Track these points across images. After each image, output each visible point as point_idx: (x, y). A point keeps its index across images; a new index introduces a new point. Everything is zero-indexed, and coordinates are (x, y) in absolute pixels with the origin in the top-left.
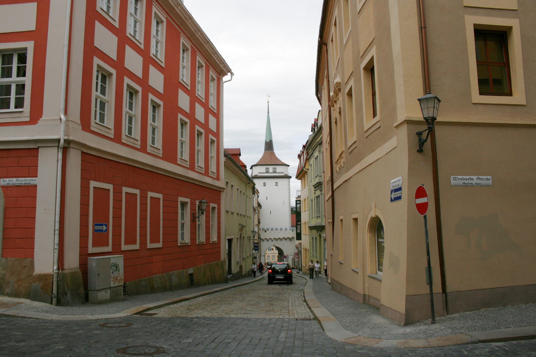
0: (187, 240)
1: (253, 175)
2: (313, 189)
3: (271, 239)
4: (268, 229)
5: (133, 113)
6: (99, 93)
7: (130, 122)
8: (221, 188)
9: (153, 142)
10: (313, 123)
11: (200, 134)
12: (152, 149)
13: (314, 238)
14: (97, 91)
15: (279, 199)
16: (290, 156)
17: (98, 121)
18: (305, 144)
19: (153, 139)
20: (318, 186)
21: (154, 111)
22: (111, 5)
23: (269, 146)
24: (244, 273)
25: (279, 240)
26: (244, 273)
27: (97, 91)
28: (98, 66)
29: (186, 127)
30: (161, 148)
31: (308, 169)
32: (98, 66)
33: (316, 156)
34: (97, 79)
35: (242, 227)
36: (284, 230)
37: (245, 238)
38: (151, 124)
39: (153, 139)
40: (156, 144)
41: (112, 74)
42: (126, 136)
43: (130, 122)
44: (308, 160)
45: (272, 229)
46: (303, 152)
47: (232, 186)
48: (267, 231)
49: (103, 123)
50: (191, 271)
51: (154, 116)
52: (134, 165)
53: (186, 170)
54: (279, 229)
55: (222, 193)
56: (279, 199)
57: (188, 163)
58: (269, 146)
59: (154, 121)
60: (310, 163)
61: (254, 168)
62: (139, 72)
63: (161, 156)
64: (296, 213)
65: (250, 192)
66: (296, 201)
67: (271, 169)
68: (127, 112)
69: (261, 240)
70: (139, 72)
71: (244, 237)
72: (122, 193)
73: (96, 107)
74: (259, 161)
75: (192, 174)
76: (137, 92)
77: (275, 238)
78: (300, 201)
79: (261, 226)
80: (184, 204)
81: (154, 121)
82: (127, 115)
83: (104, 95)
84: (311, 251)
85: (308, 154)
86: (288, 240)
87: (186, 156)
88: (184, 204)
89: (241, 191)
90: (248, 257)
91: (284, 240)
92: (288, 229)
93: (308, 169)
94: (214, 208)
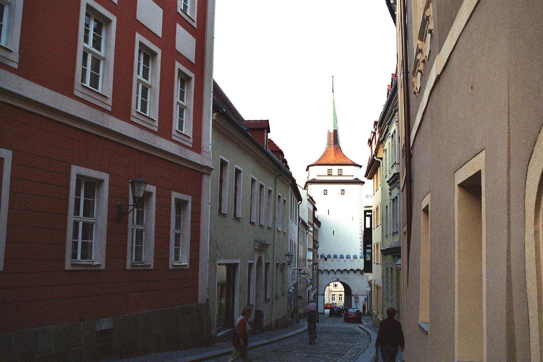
0: (148, 258)
1: (310, 179)
2: (388, 187)
3: (333, 270)
4: (329, 256)
5: (184, 104)
6: (141, 77)
7: (144, 95)
8: (203, 167)
9: (181, 127)
10: (390, 84)
11: (149, 55)
12: (177, 135)
13: (389, 269)
14: (86, 40)
15: (345, 213)
16: (358, 150)
17: (139, 110)
18: (377, 119)
19: (181, 123)
20: (393, 181)
21: (182, 86)
22: (189, 5)
23: (334, 138)
24: (265, 324)
25: (345, 274)
26: (265, 324)
27: (138, 74)
28: (141, 44)
29: (108, 31)
30: (156, 119)
31: (382, 159)
32: (141, 44)
33: (392, 132)
34: (139, 60)
35: (262, 247)
36: (352, 257)
37: (271, 266)
38: (178, 103)
39: (181, 123)
40: (148, 112)
41: (157, 54)
42: (138, 113)
43: (144, 95)
44: (381, 143)
45: (335, 257)
46: (375, 133)
47: (238, 172)
48: (329, 260)
49: (97, 88)
50: (105, 324)
51: (182, 93)
52: (158, 155)
53: (152, 135)
54: (345, 257)
55: (205, 178)
56: (345, 213)
57: (191, 141)
58: (334, 138)
59: (182, 98)
60: (385, 148)
61: (310, 168)
62: (157, 29)
63: (16, 66)
64: (367, 234)
65: (289, 195)
66: (365, 212)
67: (335, 169)
68: (139, 81)
69: (320, 273)
70: (157, 29)
71: (267, 264)
72: (171, 198)
73: (137, 94)
74: (319, 160)
75: (115, 124)
76: (189, 79)
77: (339, 270)
78: (371, 211)
79: (320, 252)
80: (91, 186)
81: (182, 98)
82: (178, 106)
83: (147, 78)
84: (385, 291)
85: (381, 132)
86: (358, 273)
87: (188, 130)
88: (91, 186)
89: (261, 187)
90: (277, 298)
91: (352, 273)
92: (358, 257)
93: (382, 159)
94: (181, 205)
